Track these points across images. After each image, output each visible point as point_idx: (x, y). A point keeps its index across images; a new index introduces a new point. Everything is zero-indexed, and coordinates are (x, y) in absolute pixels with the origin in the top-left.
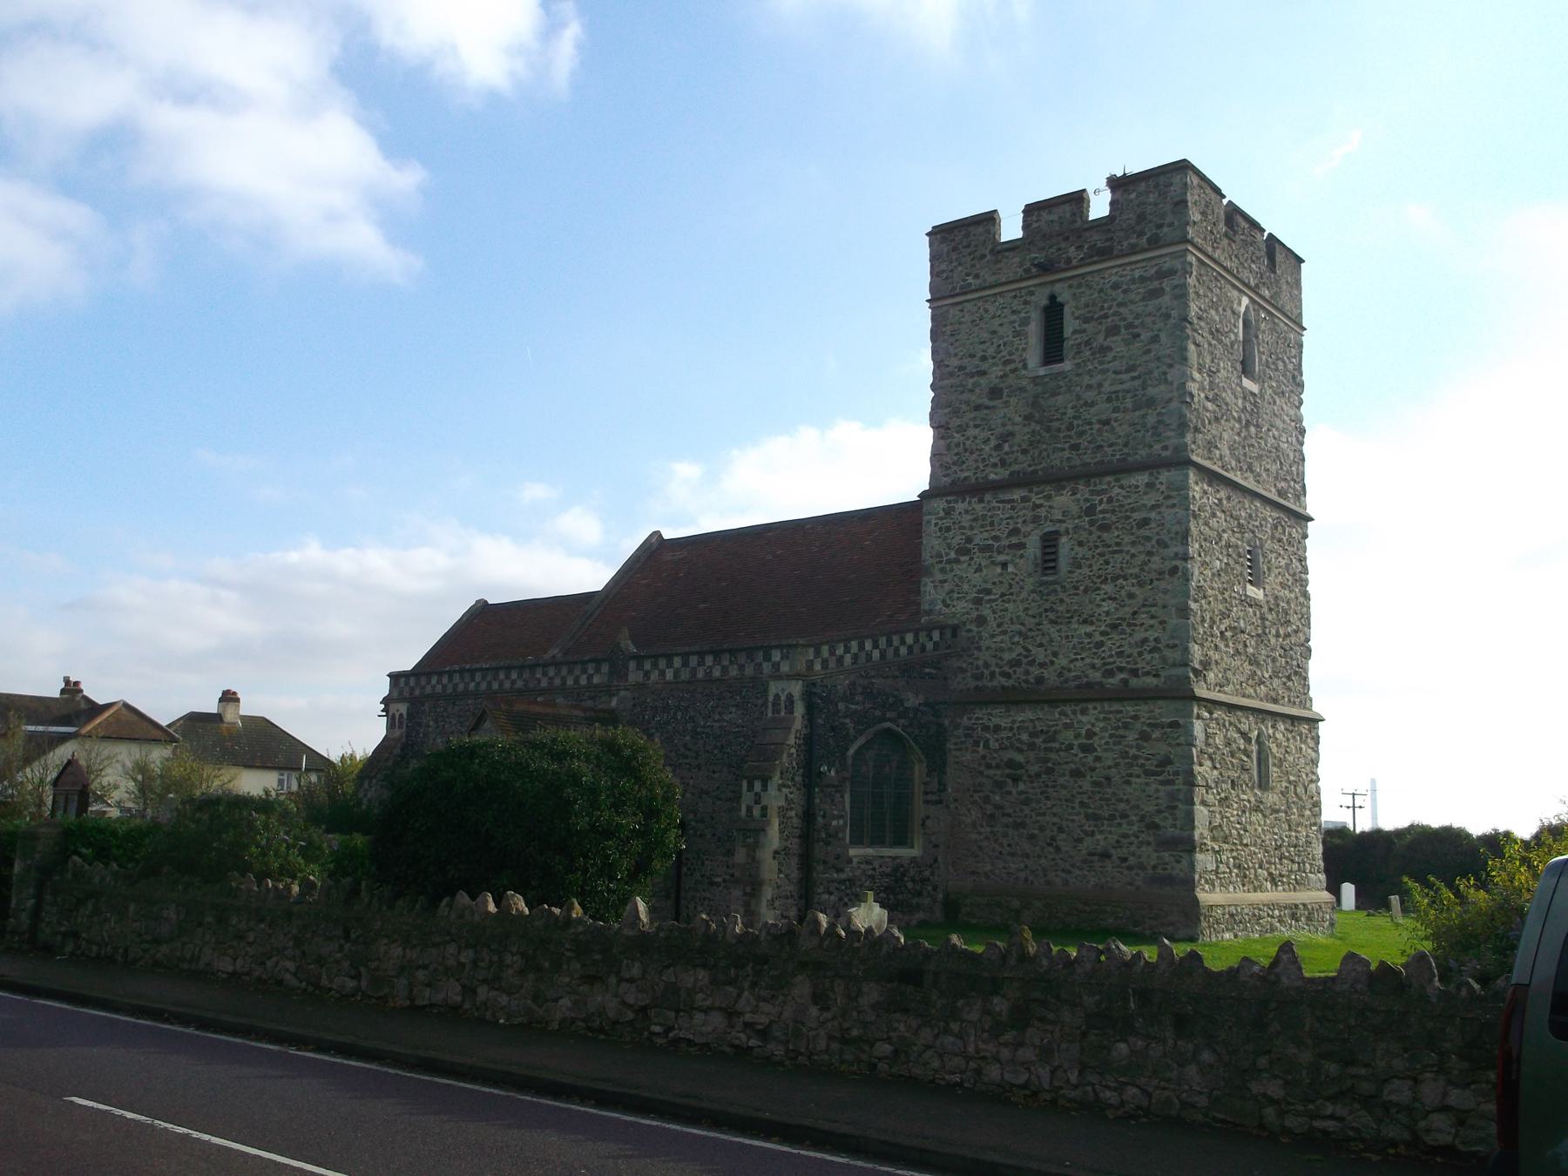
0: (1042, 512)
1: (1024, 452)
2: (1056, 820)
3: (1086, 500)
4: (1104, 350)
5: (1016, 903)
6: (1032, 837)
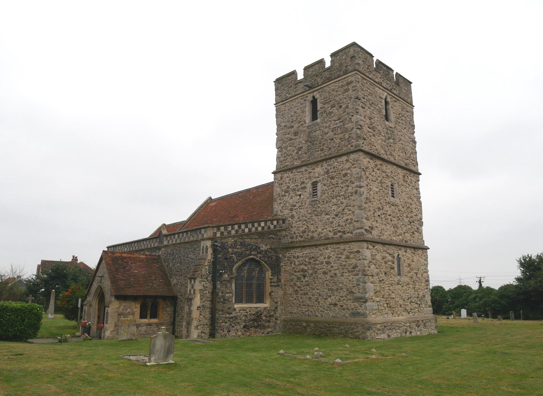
0: (312, 174)
1: (306, 153)
2: (318, 291)
3: (326, 169)
5: (304, 324)
6: (310, 298)
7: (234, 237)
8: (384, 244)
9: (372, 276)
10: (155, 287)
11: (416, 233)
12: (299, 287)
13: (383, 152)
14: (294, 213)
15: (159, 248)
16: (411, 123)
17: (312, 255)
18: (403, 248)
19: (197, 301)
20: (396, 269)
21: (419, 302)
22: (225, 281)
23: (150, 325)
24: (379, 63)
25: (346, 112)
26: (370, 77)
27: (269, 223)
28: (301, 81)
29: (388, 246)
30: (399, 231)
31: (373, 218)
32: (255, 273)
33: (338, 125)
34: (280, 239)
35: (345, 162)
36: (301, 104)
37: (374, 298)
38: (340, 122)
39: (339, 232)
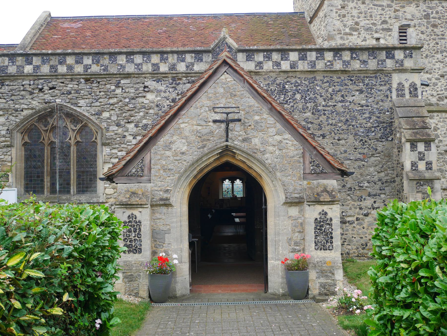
0: (400, 14)
3: (424, 11)
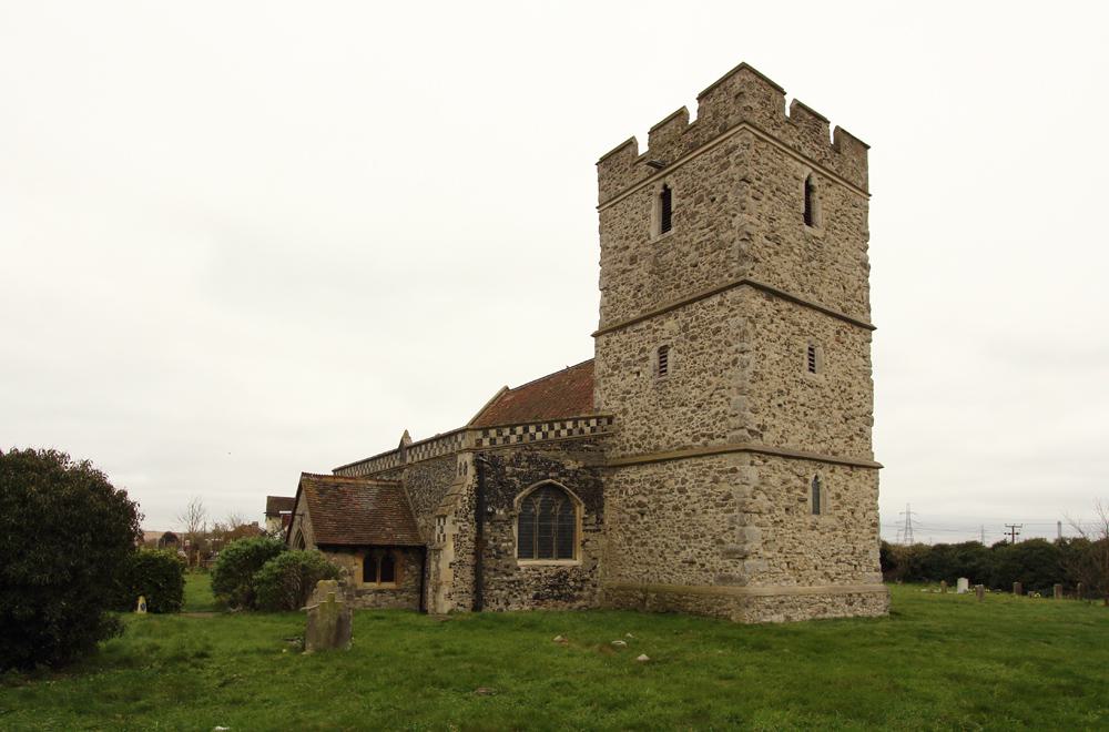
1: (649, 295)
4: (694, 215)
5: (641, 595)
6: (651, 551)
7: (515, 447)
8: (787, 457)
9: (760, 513)
10: (390, 533)
11: (857, 439)
12: (633, 533)
13: (795, 285)
14: (627, 405)
15: (400, 469)
16: (862, 229)
17: (656, 477)
18: (827, 465)
19: (449, 554)
20: (810, 502)
21: (854, 563)
22: (499, 521)
23: (381, 591)
24: (799, 107)
25: (737, 206)
26: (776, 135)
27: (581, 424)
28: (642, 159)
29: (796, 461)
30: (822, 434)
31: (767, 409)
32: (556, 510)
33: (706, 237)
34: (602, 451)
35: (716, 307)
36: (643, 202)
37: (761, 551)
38: (711, 230)
39: (703, 435)
